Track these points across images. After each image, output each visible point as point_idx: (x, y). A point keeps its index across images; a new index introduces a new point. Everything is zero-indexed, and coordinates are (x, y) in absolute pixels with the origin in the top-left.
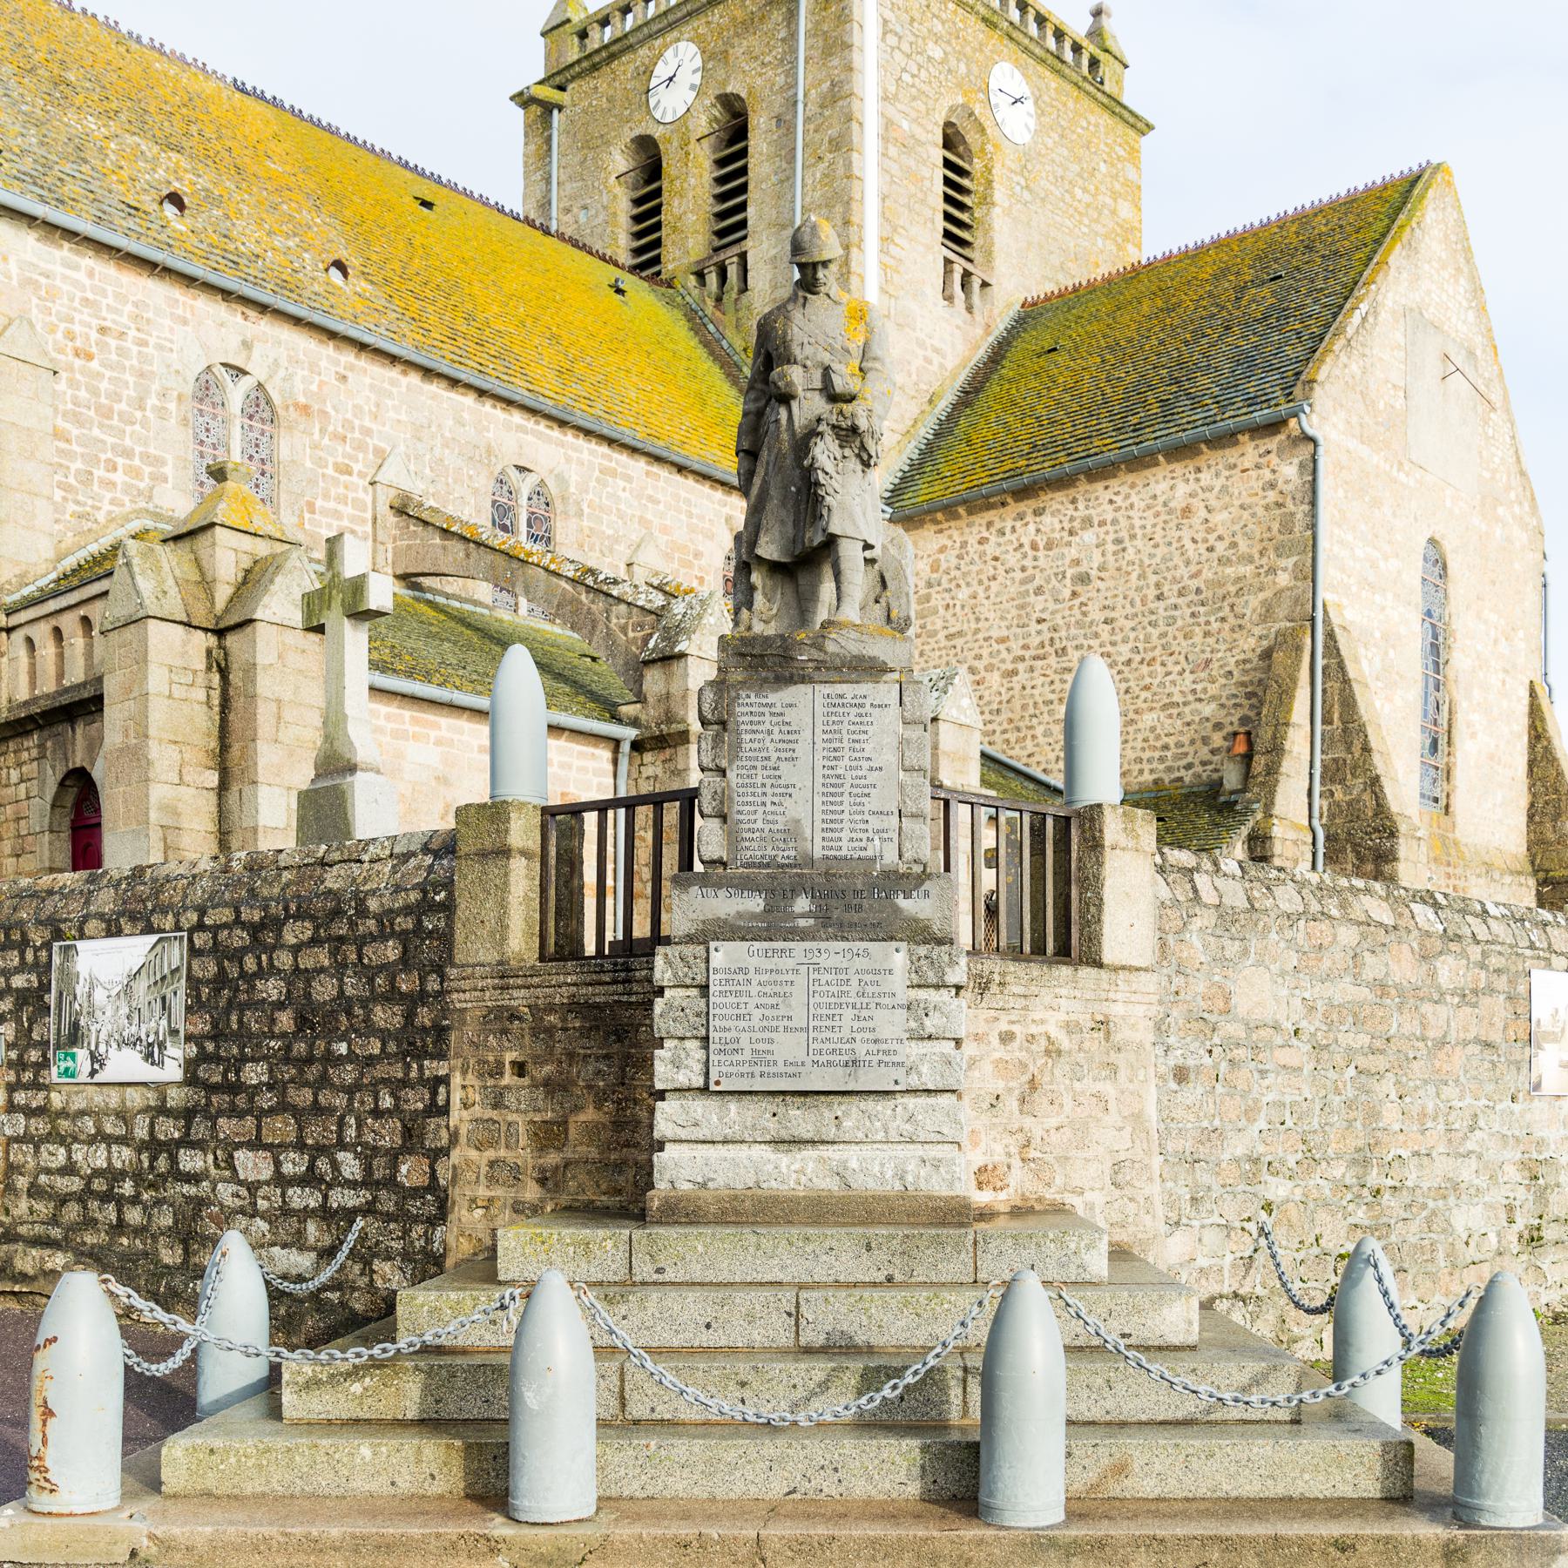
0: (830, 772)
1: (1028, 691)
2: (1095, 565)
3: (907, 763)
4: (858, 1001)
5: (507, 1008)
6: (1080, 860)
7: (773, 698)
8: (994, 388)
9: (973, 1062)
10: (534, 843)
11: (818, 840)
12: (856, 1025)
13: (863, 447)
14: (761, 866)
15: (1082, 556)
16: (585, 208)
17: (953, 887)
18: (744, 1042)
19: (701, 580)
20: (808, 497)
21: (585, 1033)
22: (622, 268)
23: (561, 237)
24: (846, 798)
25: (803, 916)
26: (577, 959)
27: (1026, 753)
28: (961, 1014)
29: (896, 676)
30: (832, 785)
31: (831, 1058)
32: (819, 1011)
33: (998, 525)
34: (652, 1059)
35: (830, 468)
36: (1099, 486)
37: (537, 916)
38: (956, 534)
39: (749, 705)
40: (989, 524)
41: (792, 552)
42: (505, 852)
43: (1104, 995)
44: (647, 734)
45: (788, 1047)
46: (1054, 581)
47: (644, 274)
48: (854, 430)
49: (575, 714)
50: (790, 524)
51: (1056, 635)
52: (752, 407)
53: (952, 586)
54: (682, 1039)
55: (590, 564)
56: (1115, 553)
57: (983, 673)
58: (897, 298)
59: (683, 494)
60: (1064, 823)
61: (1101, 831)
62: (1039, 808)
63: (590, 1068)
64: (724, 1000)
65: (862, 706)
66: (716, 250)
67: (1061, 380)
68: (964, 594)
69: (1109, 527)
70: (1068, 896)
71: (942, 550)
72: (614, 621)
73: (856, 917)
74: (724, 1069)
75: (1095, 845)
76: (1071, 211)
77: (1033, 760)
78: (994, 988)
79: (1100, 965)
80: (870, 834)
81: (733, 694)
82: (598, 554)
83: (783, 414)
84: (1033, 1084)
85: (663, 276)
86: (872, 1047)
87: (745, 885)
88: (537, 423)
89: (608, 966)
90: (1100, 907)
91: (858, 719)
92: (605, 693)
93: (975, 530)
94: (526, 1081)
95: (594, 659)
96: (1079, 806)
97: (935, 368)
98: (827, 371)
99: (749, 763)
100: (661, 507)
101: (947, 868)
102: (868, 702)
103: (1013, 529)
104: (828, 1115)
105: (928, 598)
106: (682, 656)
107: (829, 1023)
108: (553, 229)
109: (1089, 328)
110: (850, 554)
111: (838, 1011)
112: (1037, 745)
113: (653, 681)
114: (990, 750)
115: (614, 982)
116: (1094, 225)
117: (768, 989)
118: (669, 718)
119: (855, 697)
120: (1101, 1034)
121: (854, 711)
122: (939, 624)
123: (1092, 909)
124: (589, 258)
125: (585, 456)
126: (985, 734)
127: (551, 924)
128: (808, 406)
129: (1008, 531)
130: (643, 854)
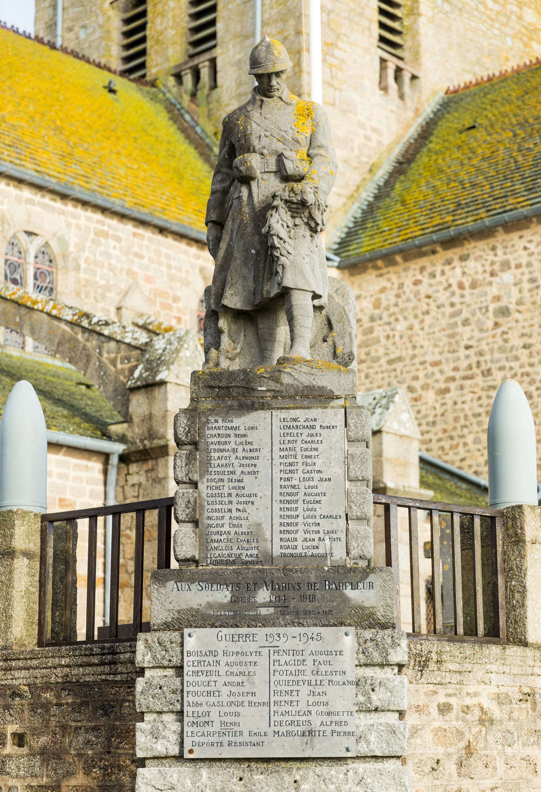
0: (287, 483)
1: (459, 406)
2: (514, 300)
3: (352, 475)
4: (313, 678)
5: (10, 687)
6: (504, 553)
7: (237, 422)
8: (423, 159)
9: (415, 731)
10: (35, 546)
11: (276, 540)
12: (312, 699)
13: (311, 217)
14: (227, 563)
15: (502, 293)
16: (84, 27)
17: (395, 580)
18: (214, 716)
19: (179, 320)
20: (265, 257)
21: (76, 708)
22: (114, 72)
23: (64, 50)
24: (300, 505)
25: (264, 605)
26: (71, 644)
27: (458, 458)
28: (403, 689)
29: (341, 402)
30: (289, 494)
31: (290, 728)
32: (279, 688)
33: (429, 269)
34: (134, 730)
35: (283, 233)
36: (515, 236)
37: (36, 607)
38: (394, 277)
39: (217, 429)
40: (422, 269)
41: (252, 300)
42: (10, 554)
43: (529, 670)
44: (133, 449)
45: (252, 720)
46: (478, 315)
47: (132, 77)
48: (303, 204)
49: (71, 433)
50: (251, 279)
51: (482, 359)
52: (219, 187)
53: (392, 320)
54: (160, 713)
55: (86, 309)
56: (530, 290)
57: (420, 392)
58: (340, 90)
59: (164, 250)
60: (489, 523)
61: (522, 528)
62: (467, 510)
63: (81, 738)
64: (197, 679)
65: (313, 427)
66: (192, 57)
67: (480, 151)
68: (401, 326)
69: (524, 269)
70: (496, 585)
71: (383, 290)
72: (105, 355)
73: (310, 606)
74: (196, 739)
75: (517, 540)
76: (484, 18)
77: (465, 464)
78: (432, 666)
79: (525, 644)
80: (322, 535)
81: (204, 419)
82: (92, 300)
83: (244, 192)
84: (469, 750)
85: (148, 78)
86: (326, 719)
87: (214, 580)
88: (43, 196)
89: (96, 650)
90: (523, 592)
91: (309, 439)
92: (97, 414)
93: (410, 273)
94: (25, 750)
95: (88, 387)
96: (502, 507)
97: (373, 144)
98: (280, 157)
99: (217, 477)
100: (145, 261)
101: (389, 563)
102: (318, 424)
103: (443, 273)
104: (288, 779)
105: (371, 330)
106: (163, 383)
107: (288, 698)
108: (59, 43)
109: (502, 109)
110: (302, 303)
111: (296, 688)
112: (468, 451)
113: (138, 405)
114: (427, 456)
115: (102, 664)
116: (503, 28)
117: (235, 669)
118: (152, 435)
119: (307, 420)
120: (529, 705)
121: (306, 432)
122: (381, 351)
123: (517, 595)
124: (87, 66)
125: (83, 222)
126: (423, 442)
127: (49, 614)
128: (265, 186)
129: (438, 274)
130: (128, 549)
